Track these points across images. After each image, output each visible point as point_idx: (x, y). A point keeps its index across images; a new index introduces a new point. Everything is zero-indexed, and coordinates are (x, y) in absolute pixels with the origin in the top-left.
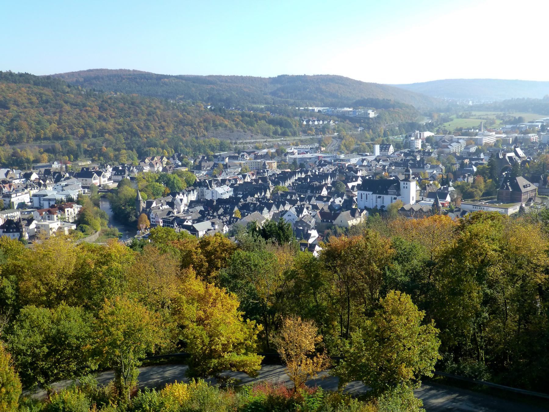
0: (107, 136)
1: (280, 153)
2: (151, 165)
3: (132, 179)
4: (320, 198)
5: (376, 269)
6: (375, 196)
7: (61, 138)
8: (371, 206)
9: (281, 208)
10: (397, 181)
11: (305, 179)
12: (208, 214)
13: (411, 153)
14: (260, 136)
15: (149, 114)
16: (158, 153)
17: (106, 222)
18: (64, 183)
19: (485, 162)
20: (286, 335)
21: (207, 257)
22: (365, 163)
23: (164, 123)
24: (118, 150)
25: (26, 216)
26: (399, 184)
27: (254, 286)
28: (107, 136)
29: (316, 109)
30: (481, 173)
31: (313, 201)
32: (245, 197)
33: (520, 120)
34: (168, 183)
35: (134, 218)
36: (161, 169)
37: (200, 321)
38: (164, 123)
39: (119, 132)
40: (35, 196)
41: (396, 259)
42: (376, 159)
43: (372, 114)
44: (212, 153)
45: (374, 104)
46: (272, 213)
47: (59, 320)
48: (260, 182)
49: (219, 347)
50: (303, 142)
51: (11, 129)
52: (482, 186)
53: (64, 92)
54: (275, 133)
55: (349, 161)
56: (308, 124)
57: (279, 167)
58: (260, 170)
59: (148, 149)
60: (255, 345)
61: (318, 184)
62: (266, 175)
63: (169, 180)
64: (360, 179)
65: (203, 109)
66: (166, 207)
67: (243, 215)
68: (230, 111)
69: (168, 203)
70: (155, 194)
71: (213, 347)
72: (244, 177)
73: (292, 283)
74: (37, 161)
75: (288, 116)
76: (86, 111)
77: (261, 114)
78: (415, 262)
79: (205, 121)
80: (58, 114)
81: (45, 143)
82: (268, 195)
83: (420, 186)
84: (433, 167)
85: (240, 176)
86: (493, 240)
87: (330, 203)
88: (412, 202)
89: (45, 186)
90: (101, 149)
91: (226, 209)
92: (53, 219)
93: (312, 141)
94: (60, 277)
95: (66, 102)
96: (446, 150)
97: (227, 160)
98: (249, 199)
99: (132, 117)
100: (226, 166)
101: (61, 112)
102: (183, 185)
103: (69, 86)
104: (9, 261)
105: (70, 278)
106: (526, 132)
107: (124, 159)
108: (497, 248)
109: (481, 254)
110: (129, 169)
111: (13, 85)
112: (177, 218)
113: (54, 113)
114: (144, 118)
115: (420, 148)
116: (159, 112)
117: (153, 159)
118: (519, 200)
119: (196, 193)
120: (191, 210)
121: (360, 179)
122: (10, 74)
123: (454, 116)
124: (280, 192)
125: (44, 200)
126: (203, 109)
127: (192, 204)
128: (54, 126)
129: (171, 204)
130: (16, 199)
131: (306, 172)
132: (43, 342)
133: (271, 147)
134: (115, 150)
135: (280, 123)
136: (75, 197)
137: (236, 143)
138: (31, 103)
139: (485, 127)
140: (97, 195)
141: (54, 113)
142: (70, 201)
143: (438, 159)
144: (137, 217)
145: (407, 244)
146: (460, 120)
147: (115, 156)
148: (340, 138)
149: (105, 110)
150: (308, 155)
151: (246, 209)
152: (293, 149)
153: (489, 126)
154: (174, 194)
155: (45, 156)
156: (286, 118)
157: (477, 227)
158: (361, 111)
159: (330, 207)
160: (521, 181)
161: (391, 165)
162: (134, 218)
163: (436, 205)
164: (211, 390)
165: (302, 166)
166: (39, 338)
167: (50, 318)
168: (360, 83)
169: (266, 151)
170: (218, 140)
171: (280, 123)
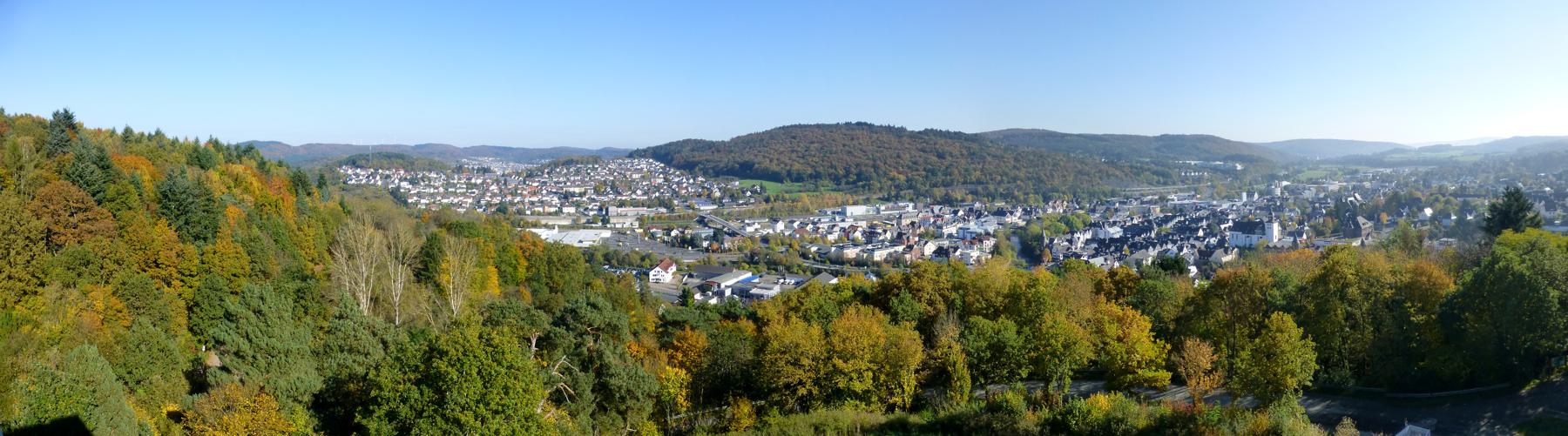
0: (1019, 182)
1: (1163, 199)
2: (1054, 208)
3: (1038, 218)
4: (1197, 238)
5: (1259, 295)
6: (1244, 235)
7: (983, 183)
8: (1241, 245)
9: (1164, 247)
10: (1262, 222)
11: (1184, 221)
12: (1102, 251)
13: (1272, 199)
14: (1145, 184)
15: (1054, 166)
16: (1059, 197)
17: (1015, 254)
18: (983, 220)
19: (1332, 205)
20: (1186, 355)
21: (1115, 286)
22: (1235, 208)
23: (1066, 173)
24: (1028, 194)
25: (953, 245)
26: (1264, 225)
27: (1159, 311)
28: (1019, 182)
29: (1193, 163)
30: (1329, 214)
31: (1192, 241)
32: (1133, 237)
33: (1356, 171)
34: (1068, 223)
35: (1038, 252)
36: (1061, 211)
37: (1120, 340)
38: (1066, 173)
39: (1029, 179)
40: (960, 228)
41: (1274, 286)
42: (1243, 205)
43: (1239, 167)
44: (1105, 199)
45: (1241, 159)
46: (1156, 251)
47: (1000, 331)
48: (1146, 224)
49: (1135, 364)
50: (1181, 190)
51: (946, 175)
52: (1331, 225)
53: (988, 147)
54: (1158, 182)
55: (1221, 206)
56: (1186, 175)
57: (1161, 211)
58: (1145, 214)
59: (1050, 194)
60: (1164, 363)
61: (1195, 226)
62: (1151, 218)
63: (1069, 221)
64: (1231, 221)
65: (1098, 161)
66: (1067, 243)
67: (1132, 253)
68: (1120, 163)
69: (1067, 240)
70: (1057, 232)
71: (1130, 364)
72: (1132, 219)
73: (1191, 309)
74: (963, 201)
75: (1170, 168)
76: (1004, 162)
77: (1146, 167)
78: (1290, 288)
79: (1100, 171)
80: (981, 164)
81: (969, 186)
82: (1153, 235)
83: (1282, 227)
84: (1291, 211)
85: (1129, 219)
86: (1350, 265)
87: (1205, 243)
88: (1275, 240)
89: (969, 221)
90: (1013, 193)
91: (1116, 247)
92: (973, 249)
93: (1189, 190)
94: (998, 294)
95: (989, 155)
96: (1301, 197)
97: (1117, 204)
98: (1137, 239)
99: (1040, 168)
100: (1116, 210)
101: (984, 162)
102: (1080, 225)
103: (991, 142)
104: (956, 278)
105: (1006, 297)
106: (1361, 181)
107: (1031, 202)
108: (1354, 272)
109: (1342, 278)
110: (1035, 210)
111: (949, 141)
112: (1075, 253)
113: (979, 163)
114: (1050, 168)
115: (1279, 194)
116: (1062, 163)
117: (1055, 202)
118: (1360, 235)
119: (1091, 233)
120: (1087, 247)
121: (1231, 221)
122: (948, 132)
123: (1305, 169)
124: (1163, 233)
125: (968, 232)
126: (1098, 161)
127: (1087, 242)
128: (978, 173)
129: (1070, 241)
130: (946, 230)
131: (1185, 216)
132: (987, 348)
133: (1155, 194)
134: (1025, 194)
135: (1163, 175)
136: (992, 232)
137: (1125, 191)
138: (962, 155)
139: (1330, 177)
140: (1009, 231)
141: (979, 163)
142: (988, 234)
143: (1294, 204)
144: (1041, 251)
145: (1282, 273)
146: (1310, 172)
147: (1025, 199)
148: (1213, 187)
149: (1019, 161)
150: (1186, 202)
151: (1135, 247)
152: (1173, 197)
153: (1332, 176)
154: (1072, 233)
155: (970, 197)
156: (1167, 170)
157: (1336, 256)
158: (1230, 164)
159: (1207, 246)
160: (1361, 220)
161: (1256, 209)
162: (1038, 252)
163: (1295, 241)
164: (1129, 402)
165: (1181, 210)
166: (985, 344)
167: (992, 328)
168: (1228, 141)
169: (1150, 197)
170: (1110, 188)
171: (1163, 175)
